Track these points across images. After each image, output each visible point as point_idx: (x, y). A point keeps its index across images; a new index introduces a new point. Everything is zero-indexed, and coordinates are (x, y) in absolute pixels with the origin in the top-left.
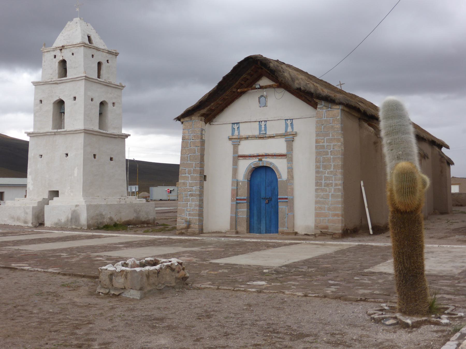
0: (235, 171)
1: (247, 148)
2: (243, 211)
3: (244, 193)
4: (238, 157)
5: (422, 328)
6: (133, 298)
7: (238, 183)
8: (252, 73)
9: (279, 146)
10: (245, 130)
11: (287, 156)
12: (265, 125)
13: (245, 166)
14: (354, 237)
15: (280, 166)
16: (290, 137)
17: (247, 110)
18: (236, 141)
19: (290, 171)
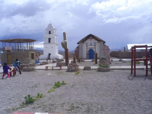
0: (87, 50)
1: (88, 47)
2: (88, 56)
3: (88, 53)
4: (87, 48)
5: (31, 73)
6: (135, 46)
7: (30, 41)
8: (90, 37)
9: (94, 47)
10: (88, 44)
11: (95, 48)
12: (143, 69)
13: (88, 49)
14: (37, 48)
15: (94, 49)
16: (95, 46)
17: (88, 41)
18: (87, 46)
19: (95, 50)
